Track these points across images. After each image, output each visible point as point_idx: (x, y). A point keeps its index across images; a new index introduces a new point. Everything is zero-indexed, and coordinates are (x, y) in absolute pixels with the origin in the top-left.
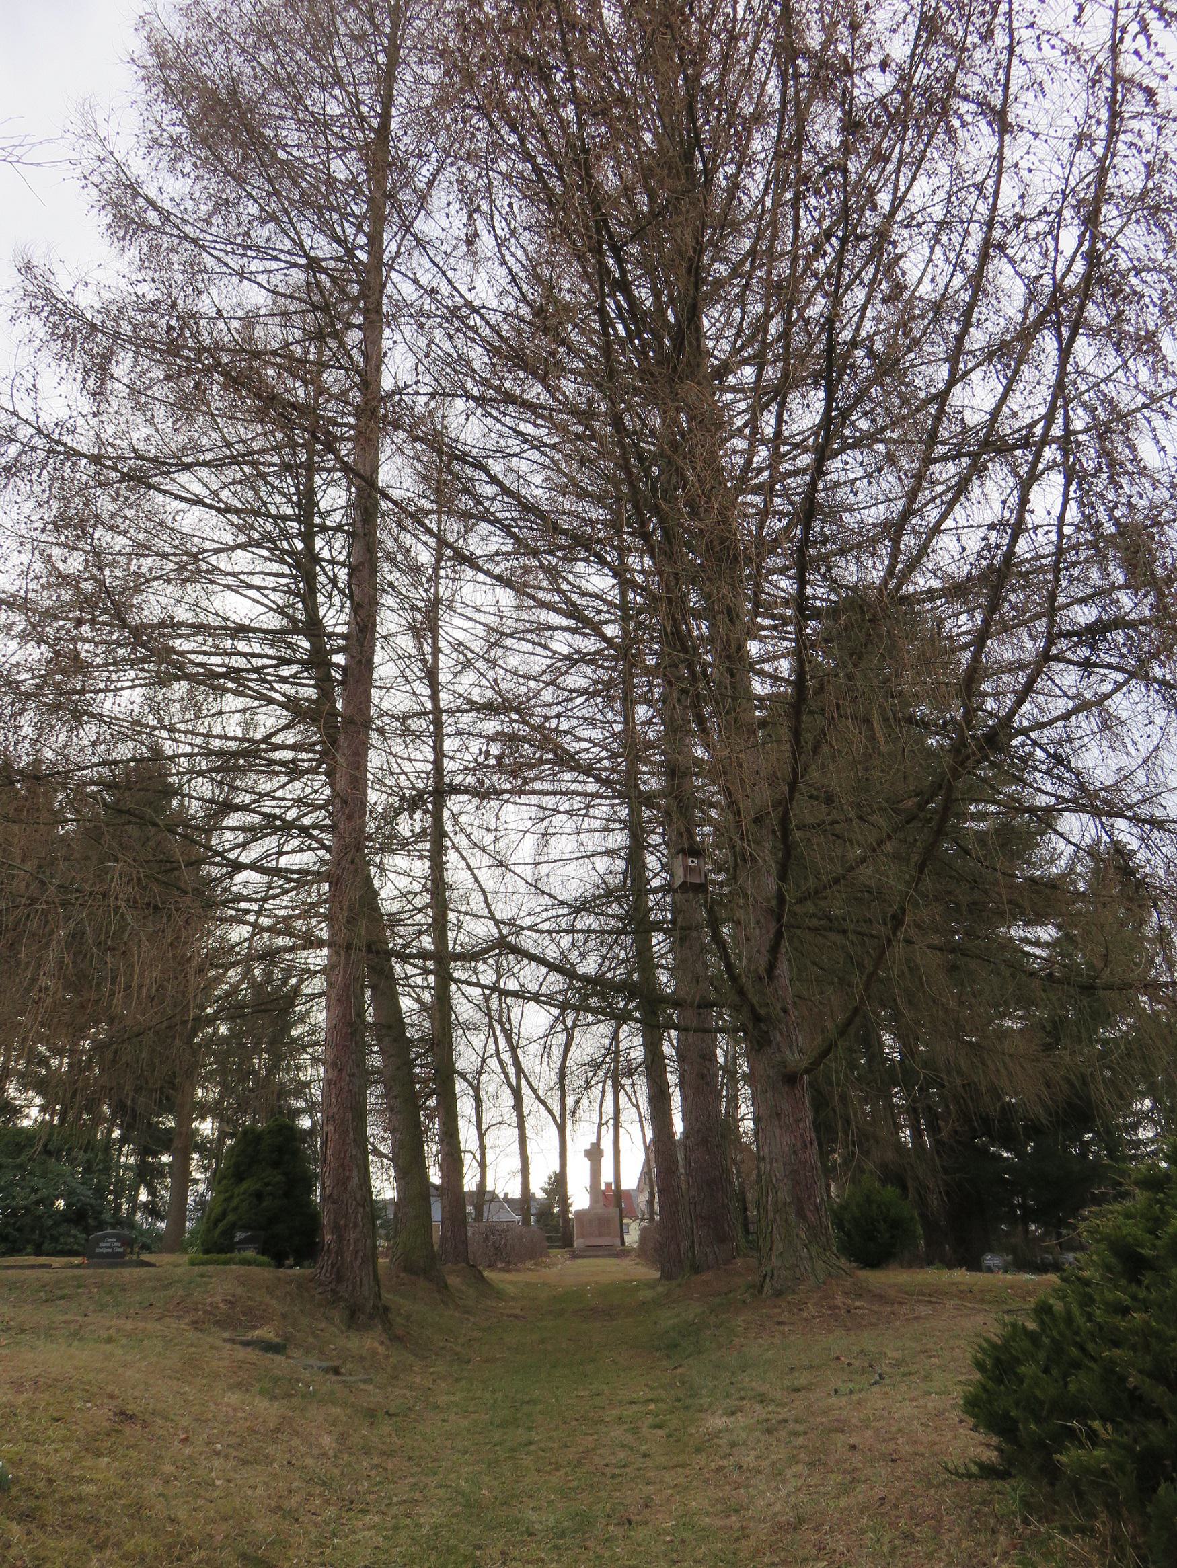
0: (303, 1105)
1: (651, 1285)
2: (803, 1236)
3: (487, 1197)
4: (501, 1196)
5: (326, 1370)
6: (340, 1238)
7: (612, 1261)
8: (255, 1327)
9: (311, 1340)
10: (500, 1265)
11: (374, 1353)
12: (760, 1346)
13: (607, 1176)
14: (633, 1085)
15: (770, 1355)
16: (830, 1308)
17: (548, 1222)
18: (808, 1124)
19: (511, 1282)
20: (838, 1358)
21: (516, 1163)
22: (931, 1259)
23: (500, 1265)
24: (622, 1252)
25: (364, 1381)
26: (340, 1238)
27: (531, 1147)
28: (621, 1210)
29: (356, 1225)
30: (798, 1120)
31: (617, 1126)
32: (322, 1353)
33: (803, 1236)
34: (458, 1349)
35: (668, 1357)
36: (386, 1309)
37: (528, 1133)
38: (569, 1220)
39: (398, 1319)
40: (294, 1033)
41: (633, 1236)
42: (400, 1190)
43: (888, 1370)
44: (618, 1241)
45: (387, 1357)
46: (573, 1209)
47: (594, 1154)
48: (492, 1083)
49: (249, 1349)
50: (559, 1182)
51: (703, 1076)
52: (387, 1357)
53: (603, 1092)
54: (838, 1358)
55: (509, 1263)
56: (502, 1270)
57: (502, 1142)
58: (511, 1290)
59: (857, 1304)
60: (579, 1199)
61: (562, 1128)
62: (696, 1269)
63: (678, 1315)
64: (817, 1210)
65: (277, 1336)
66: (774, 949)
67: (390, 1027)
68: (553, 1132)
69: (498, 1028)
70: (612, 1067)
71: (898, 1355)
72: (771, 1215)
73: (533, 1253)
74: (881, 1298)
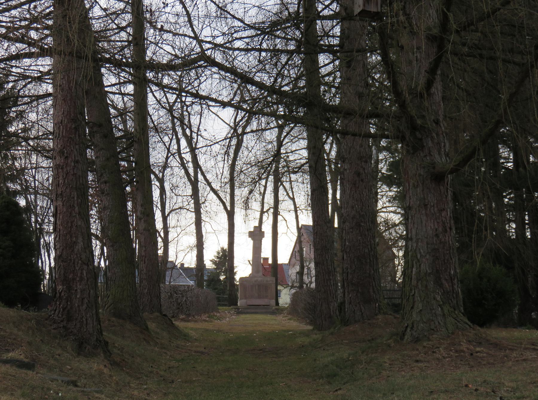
0: (19, 188)
1: (306, 334)
2: (438, 298)
3: (169, 266)
4: (179, 266)
5: (68, 383)
6: (69, 288)
7: (269, 317)
8: (8, 351)
9: (52, 362)
10: (182, 317)
11: (101, 373)
12: (404, 377)
13: (266, 252)
14: (291, 182)
15: (412, 382)
16: (456, 351)
17: (216, 284)
18: (448, 213)
19: (192, 329)
20: (466, 386)
21: (193, 240)
22: (523, 322)
23: (182, 317)
24: (277, 310)
25: (97, 392)
26: (69, 288)
27: (206, 228)
28: (277, 280)
29: (82, 279)
30: (441, 210)
31: (276, 214)
32: (61, 371)
33: (438, 298)
34: (162, 373)
35: (329, 383)
36: (106, 343)
37: (203, 217)
38: (235, 285)
39: (116, 351)
40: (12, 129)
41: (285, 297)
42: (314, 221)
43: (506, 394)
44: (273, 302)
45: (111, 376)
46: (237, 277)
47: (256, 235)
48: (175, 176)
49: (8, 366)
50: (226, 257)
51: (359, 174)
52: (111, 376)
53: (265, 187)
54: (466, 386)
55: (189, 315)
56: (183, 320)
57: (183, 223)
58: (192, 333)
59: (478, 349)
60: (243, 269)
61: (231, 215)
62: (345, 322)
63: (333, 355)
64: (452, 279)
65: (26, 357)
66: (432, 71)
67: (100, 126)
68: (224, 217)
69: (179, 130)
70: (274, 168)
71: (513, 385)
72: (414, 282)
73: (206, 309)
74: (497, 345)
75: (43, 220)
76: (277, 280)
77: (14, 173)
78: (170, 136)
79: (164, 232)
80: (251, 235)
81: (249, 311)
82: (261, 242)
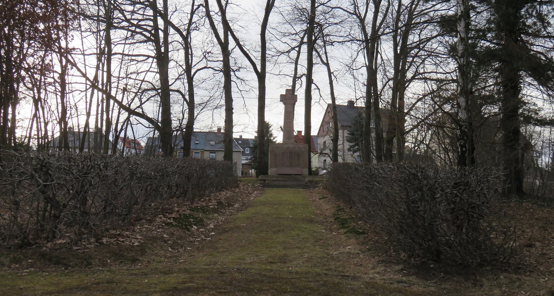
13: (299, 126)
28: (310, 147)
47: (289, 99)
61: (261, 77)
75: (127, 20)
76: (310, 147)
77: (9, 30)
78: (88, 86)
79: (189, 95)
80: (283, 98)
81: (277, 183)
82: (294, 107)
